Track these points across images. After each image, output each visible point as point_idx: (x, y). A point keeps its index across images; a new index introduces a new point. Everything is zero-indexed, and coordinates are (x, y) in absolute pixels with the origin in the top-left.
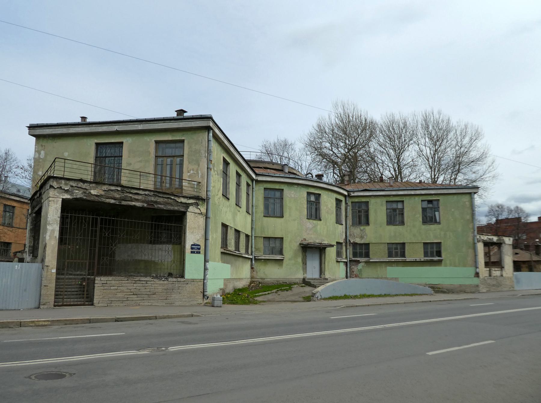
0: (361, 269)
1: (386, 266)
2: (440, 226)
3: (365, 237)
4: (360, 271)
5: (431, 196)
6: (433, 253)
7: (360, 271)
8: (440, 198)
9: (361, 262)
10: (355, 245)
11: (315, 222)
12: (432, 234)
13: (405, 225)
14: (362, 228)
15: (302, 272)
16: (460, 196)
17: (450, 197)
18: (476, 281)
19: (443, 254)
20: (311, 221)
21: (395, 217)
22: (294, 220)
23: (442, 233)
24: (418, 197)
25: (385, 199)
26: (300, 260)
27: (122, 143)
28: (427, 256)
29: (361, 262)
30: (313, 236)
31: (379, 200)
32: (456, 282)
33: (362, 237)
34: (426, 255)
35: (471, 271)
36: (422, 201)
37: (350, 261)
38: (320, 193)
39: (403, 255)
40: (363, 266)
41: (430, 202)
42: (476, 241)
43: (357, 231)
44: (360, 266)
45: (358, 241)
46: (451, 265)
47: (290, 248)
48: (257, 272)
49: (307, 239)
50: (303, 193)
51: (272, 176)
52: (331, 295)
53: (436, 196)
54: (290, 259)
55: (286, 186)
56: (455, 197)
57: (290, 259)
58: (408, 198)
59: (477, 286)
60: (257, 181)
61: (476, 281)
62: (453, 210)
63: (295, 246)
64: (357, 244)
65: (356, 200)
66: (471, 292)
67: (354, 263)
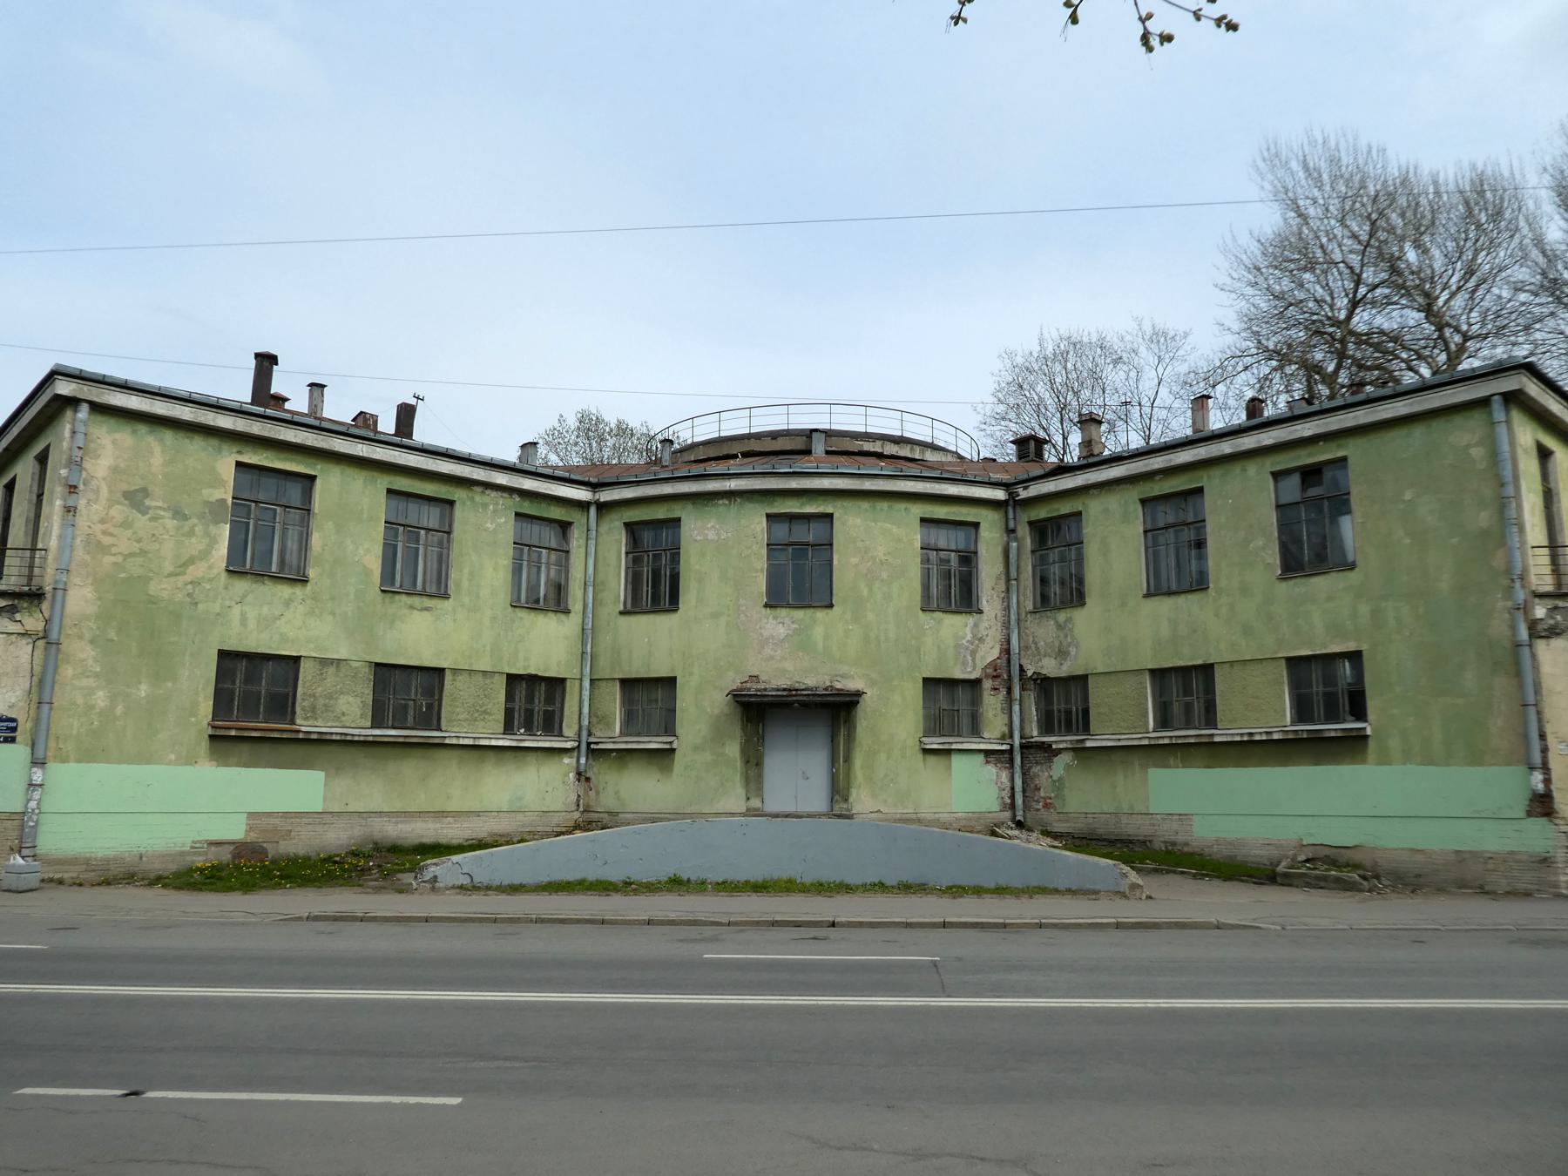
0: (1060, 779)
1: (1145, 767)
2: (1353, 577)
3: (1073, 651)
4: (1059, 785)
5: (1310, 449)
6: (1331, 705)
7: (1059, 785)
8: (1351, 450)
9: (1059, 751)
10: (1043, 684)
11: (799, 614)
12: (1321, 615)
13: (1211, 592)
14: (1062, 616)
15: (740, 791)
16: (1438, 425)
17: (1395, 437)
18: (1536, 836)
19: (1373, 704)
20: (783, 612)
21: (1179, 561)
22: (715, 616)
23: (1364, 609)
24: (1259, 460)
25: (1134, 494)
26: (733, 749)
27: (1344, 459)
28: (1311, 721)
29: (1059, 751)
30: (789, 665)
31: (1113, 502)
32: (1438, 841)
33: (1062, 654)
34: (1302, 711)
35: (1506, 786)
36: (1276, 475)
37: (1022, 746)
38: (829, 510)
39: (431, 718)
40: (1068, 767)
41: (1311, 474)
42: (1524, 634)
43: (1044, 630)
44: (1060, 765)
45: (1050, 667)
46: (1407, 757)
47: (700, 709)
48: (598, 793)
49: (762, 678)
50: (753, 524)
51: (638, 483)
52: (544, 879)
53: (1333, 445)
54: (696, 749)
55: (689, 506)
56: (1418, 431)
57: (696, 749)
58: (1216, 472)
59: (1545, 861)
60: (603, 508)
61: (1536, 836)
62: (1408, 496)
63: (717, 701)
64: (1046, 679)
65: (1042, 513)
66: (1512, 894)
67: (1040, 756)
